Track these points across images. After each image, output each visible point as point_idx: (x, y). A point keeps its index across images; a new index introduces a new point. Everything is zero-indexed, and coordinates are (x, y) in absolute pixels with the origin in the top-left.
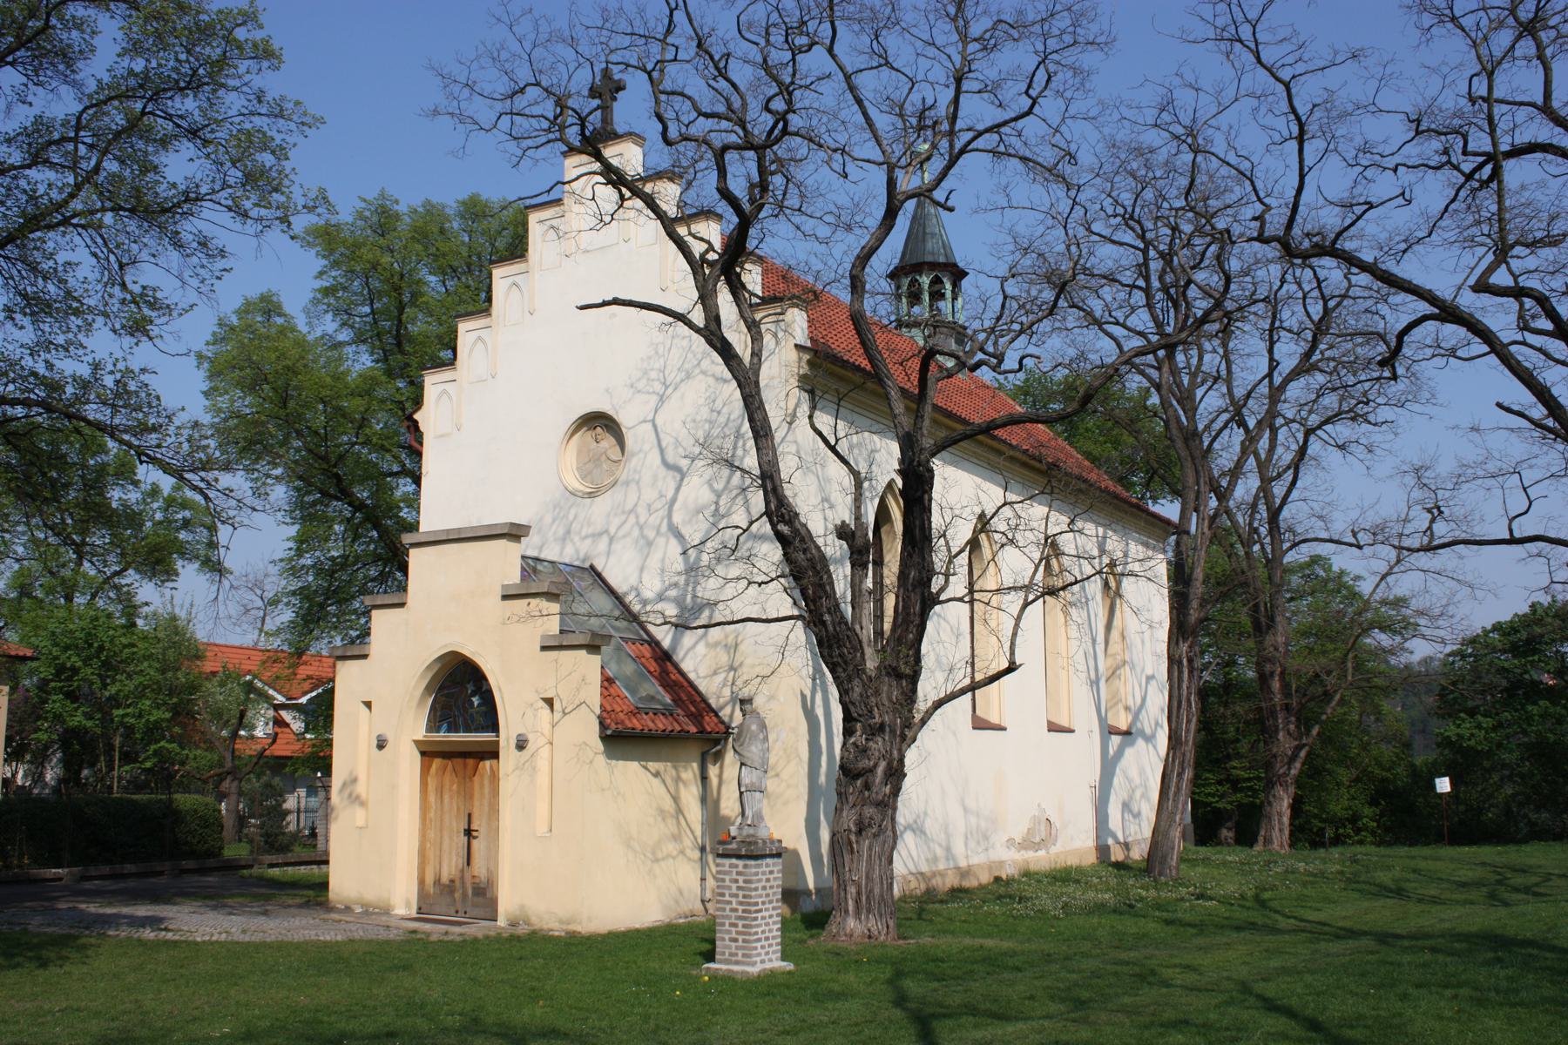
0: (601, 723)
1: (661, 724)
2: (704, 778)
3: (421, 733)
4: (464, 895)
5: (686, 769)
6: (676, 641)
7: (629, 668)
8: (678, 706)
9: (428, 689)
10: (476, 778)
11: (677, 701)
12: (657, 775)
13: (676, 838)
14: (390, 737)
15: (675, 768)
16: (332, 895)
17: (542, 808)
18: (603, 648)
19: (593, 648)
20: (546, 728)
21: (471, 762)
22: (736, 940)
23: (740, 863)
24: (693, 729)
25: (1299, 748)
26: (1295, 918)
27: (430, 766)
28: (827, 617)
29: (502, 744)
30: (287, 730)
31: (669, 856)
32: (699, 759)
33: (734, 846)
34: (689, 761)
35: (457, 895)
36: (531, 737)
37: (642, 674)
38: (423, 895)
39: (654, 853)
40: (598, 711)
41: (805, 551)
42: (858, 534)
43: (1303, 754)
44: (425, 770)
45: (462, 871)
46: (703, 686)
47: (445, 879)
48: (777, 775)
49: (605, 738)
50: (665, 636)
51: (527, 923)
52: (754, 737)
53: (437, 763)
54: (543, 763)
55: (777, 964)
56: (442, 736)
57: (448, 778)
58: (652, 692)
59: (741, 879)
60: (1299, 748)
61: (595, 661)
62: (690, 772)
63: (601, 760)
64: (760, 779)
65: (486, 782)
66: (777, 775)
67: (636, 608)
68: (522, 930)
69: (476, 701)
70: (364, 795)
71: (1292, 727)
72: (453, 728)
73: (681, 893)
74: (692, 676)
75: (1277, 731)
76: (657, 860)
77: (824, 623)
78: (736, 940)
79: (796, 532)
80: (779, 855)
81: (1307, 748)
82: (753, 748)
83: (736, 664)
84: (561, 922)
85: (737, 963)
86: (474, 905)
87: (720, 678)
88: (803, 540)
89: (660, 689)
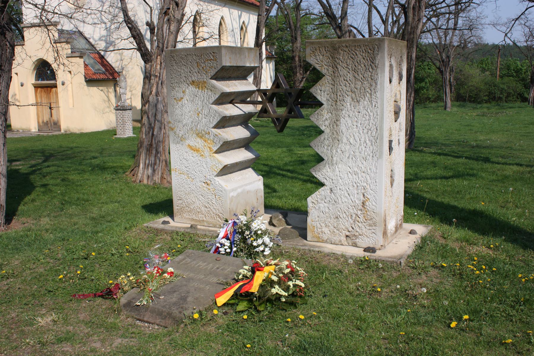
0: (85, 77)
1: (102, 77)
2: (115, 91)
3: (33, 81)
4: (51, 125)
5: (110, 88)
6: (105, 54)
7: (92, 61)
8: (106, 71)
9: (34, 69)
10: (51, 93)
11: (107, 70)
12: (102, 90)
13: (109, 107)
14: (24, 82)
15: (107, 88)
16: (12, 127)
17: (71, 101)
18: (84, 57)
19: (81, 57)
20: (70, 79)
21: (49, 89)
22: (121, 130)
23: (121, 111)
24: (111, 78)
25: (303, 78)
26: (517, 164)
27: (37, 91)
28: (143, 49)
29: (58, 84)
30: (309, 121)
31: (107, 112)
32: (113, 85)
33: (119, 108)
34: (111, 86)
35: (49, 125)
36: (66, 82)
37: (95, 63)
38: (39, 126)
39: (103, 111)
40: (84, 74)
41: (135, 32)
42: (151, 25)
43: (304, 80)
44: (36, 92)
45: (50, 119)
46: (113, 65)
47: (45, 121)
48: (135, 89)
49: (86, 81)
50: (102, 53)
51: (69, 131)
52: (123, 81)
53: (39, 89)
54: (70, 88)
55: (131, 135)
56: (40, 82)
57: (43, 93)
58: (99, 68)
59: (121, 115)
60: (303, 78)
61: (81, 61)
62: (111, 90)
63: (86, 87)
64: (125, 91)
65: (54, 95)
66: (135, 89)
67: (93, 43)
68: (68, 132)
69: (49, 72)
70: (19, 99)
71: (301, 72)
72: (43, 80)
73: (111, 122)
74: (110, 62)
75: (297, 73)
76: (104, 113)
77: (142, 50)
78: (121, 130)
79: (133, 26)
80: (131, 109)
81: (305, 78)
82: (123, 84)
83: (122, 59)
84: (79, 130)
85: (122, 135)
86: (54, 128)
87: (118, 63)
88: (135, 28)
89: (101, 67)
